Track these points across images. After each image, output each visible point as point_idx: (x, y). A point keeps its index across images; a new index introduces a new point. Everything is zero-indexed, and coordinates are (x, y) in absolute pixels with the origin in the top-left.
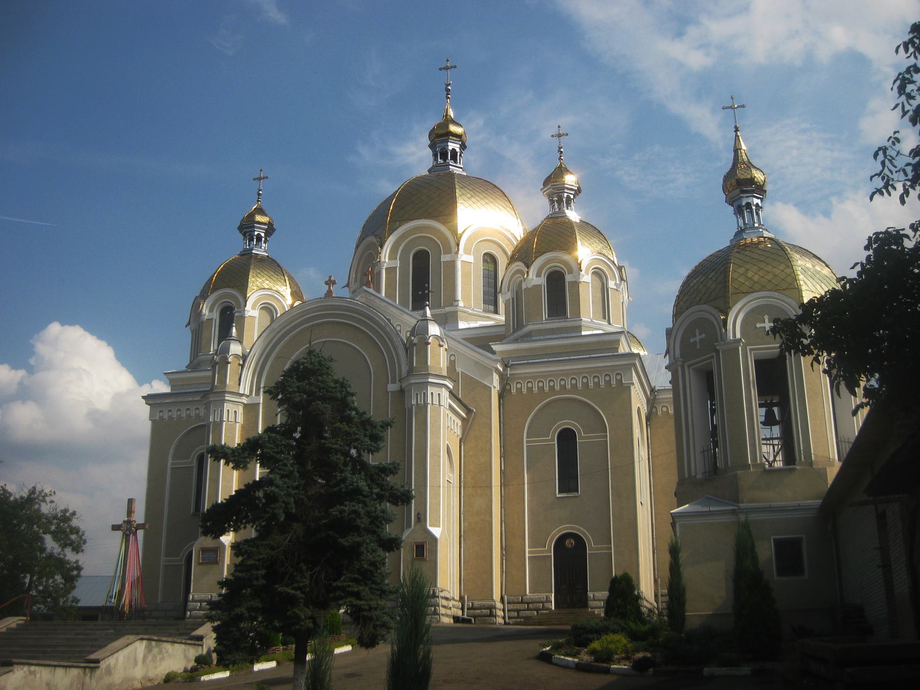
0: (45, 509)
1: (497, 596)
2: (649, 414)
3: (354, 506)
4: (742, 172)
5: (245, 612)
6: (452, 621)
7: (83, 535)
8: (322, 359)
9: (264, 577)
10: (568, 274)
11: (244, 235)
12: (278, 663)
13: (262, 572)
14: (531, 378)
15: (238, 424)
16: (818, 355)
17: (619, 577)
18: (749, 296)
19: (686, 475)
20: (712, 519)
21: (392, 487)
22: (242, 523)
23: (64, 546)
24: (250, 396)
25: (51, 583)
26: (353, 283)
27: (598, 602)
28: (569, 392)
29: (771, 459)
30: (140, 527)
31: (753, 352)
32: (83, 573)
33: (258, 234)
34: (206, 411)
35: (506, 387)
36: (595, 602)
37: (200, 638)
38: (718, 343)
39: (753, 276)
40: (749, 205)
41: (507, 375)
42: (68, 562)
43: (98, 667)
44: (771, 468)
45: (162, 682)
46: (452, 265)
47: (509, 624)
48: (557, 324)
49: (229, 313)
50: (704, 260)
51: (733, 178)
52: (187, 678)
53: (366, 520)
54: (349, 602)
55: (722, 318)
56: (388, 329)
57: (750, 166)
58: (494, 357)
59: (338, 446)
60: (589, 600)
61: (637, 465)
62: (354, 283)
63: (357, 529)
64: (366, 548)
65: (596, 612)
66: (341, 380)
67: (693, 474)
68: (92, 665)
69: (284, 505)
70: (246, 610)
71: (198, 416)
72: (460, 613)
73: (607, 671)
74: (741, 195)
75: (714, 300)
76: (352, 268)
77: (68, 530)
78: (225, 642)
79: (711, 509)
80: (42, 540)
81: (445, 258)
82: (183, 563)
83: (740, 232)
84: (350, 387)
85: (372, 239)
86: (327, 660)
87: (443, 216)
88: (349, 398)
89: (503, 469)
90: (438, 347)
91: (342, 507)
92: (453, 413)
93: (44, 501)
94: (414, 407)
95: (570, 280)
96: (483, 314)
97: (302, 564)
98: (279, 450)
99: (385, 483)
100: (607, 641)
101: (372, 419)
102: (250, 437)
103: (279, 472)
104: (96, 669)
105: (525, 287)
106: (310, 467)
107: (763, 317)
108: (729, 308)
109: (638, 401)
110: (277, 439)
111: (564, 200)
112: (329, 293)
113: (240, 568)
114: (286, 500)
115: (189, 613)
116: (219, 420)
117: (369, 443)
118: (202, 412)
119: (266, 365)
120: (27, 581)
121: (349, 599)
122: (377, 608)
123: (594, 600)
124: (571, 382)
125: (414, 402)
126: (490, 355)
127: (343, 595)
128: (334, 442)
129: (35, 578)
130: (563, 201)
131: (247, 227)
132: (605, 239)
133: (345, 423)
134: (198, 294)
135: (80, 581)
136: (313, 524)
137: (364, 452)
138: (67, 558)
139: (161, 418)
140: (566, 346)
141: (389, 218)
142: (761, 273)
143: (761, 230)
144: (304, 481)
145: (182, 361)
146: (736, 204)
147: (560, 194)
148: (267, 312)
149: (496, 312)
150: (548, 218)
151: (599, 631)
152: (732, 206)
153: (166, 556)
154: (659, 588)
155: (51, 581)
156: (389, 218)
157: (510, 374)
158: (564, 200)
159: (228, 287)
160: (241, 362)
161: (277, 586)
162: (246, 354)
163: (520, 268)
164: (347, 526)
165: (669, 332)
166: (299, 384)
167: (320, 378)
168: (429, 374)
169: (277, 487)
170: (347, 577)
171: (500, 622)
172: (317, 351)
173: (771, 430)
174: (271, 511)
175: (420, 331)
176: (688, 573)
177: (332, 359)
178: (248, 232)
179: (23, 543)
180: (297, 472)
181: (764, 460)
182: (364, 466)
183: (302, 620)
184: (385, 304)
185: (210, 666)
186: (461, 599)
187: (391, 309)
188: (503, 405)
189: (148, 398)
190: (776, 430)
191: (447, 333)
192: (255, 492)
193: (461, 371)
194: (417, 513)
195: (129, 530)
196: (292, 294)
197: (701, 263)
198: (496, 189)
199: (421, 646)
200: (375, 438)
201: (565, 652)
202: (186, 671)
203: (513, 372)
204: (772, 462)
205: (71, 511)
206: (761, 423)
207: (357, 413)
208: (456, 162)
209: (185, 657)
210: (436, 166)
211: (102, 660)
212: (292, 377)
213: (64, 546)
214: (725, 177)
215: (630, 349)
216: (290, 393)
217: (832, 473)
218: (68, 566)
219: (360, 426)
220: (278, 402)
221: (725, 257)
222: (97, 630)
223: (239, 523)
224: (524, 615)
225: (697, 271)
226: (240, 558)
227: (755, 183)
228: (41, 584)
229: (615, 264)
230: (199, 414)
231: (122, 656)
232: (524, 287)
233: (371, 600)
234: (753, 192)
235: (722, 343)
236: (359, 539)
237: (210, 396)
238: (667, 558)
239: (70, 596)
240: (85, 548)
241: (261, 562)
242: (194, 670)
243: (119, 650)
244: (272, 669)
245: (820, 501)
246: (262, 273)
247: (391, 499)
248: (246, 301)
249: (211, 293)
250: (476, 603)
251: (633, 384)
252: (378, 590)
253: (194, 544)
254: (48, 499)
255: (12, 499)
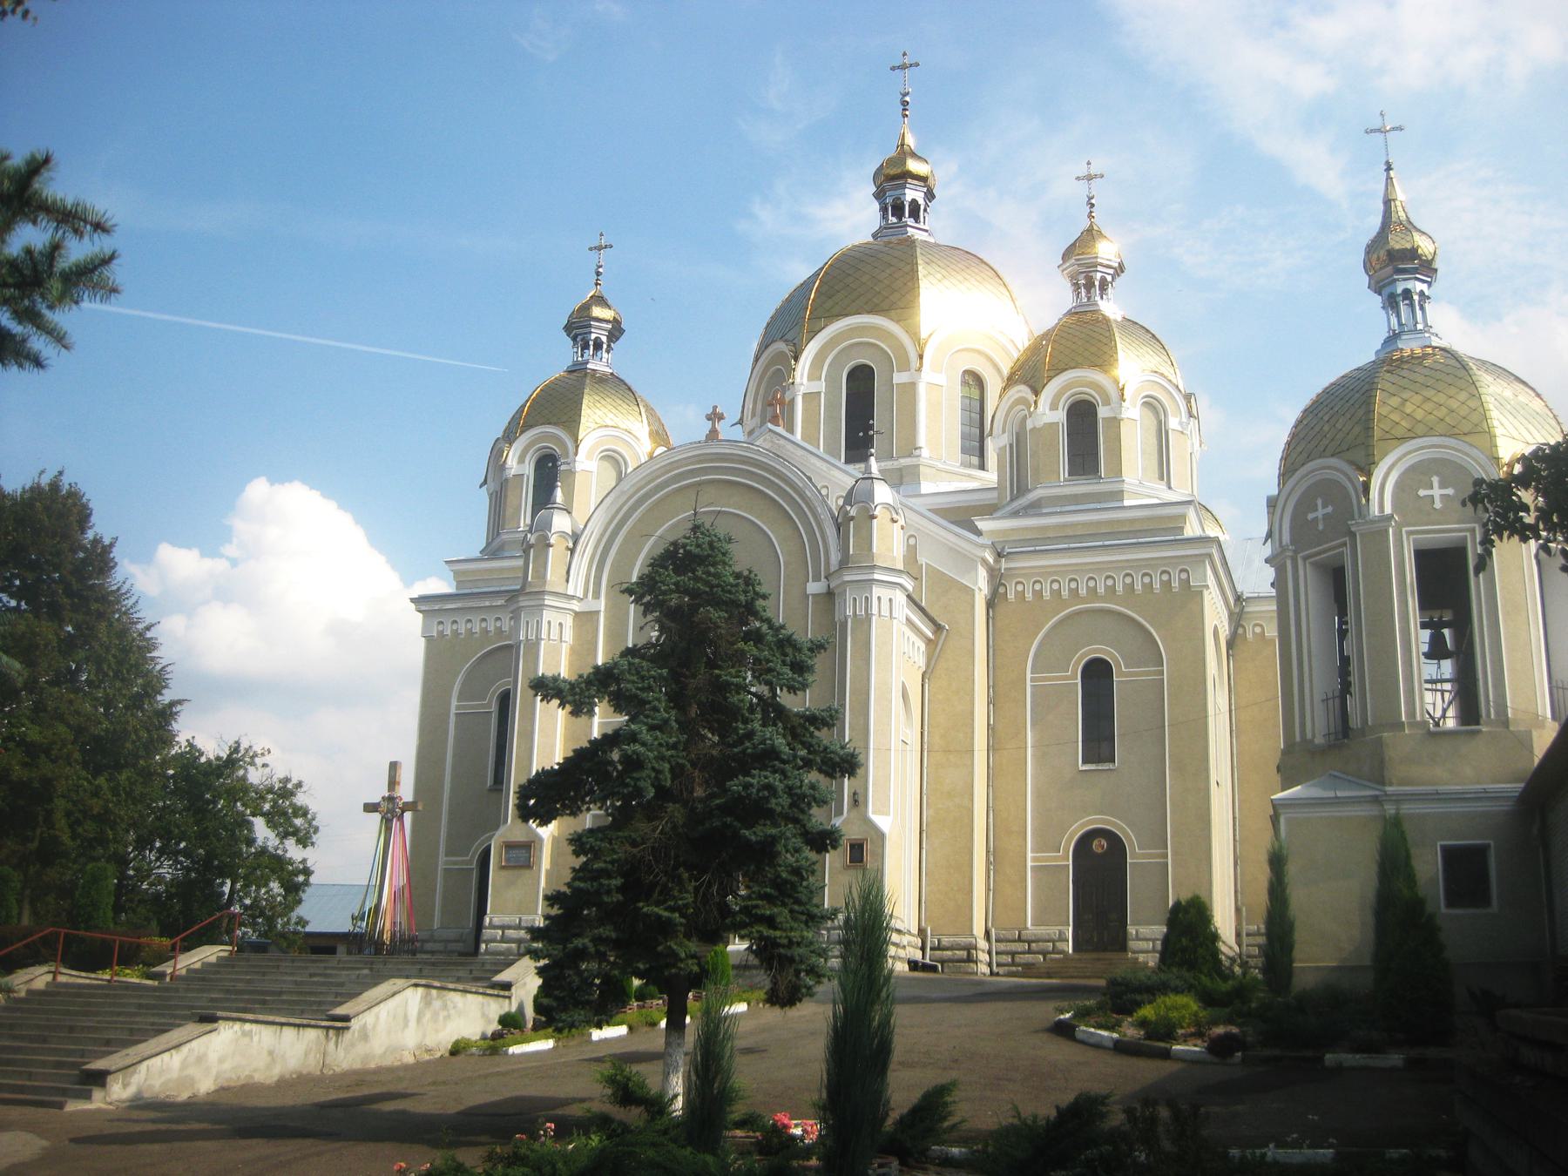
0: (255, 776)
1: (979, 929)
2: (1231, 636)
3: (766, 777)
4: (1398, 239)
5: (590, 945)
6: (906, 967)
7: (314, 819)
8: (714, 538)
9: (620, 889)
10: (1103, 405)
11: (574, 339)
12: (631, 1028)
13: (618, 882)
14: (1039, 574)
15: (564, 645)
16: (1548, 540)
17: (1183, 903)
18: (1407, 444)
19: (1298, 739)
20: (1339, 811)
21: (826, 748)
22: (584, 802)
23: (284, 836)
24: (585, 600)
25: (264, 894)
26: (750, 418)
27: (1145, 943)
28: (1084, 600)
29: (1438, 714)
30: (407, 807)
31: (1411, 537)
32: (312, 879)
33: (596, 338)
34: (512, 623)
35: (997, 590)
36: (1140, 943)
37: (507, 986)
38: (1353, 522)
39: (1414, 410)
40: (1407, 294)
41: (1000, 569)
42: (291, 862)
43: (348, 1028)
44: (1438, 729)
45: (447, 1054)
46: (911, 387)
47: (998, 974)
48: (1083, 487)
49: (550, 465)
50: (1332, 384)
51: (1382, 248)
52: (487, 1049)
53: (785, 801)
54: (758, 932)
55: (1361, 479)
56: (807, 492)
57: (1409, 227)
58: (980, 540)
59: (741, 679)
60: (1130, 940)
61: (1211, 720)
62: (752, 418)
63: (769, 815)
64: (785, 846)
65: (1141, 959)
66: (746, 573)
67: (1309, 736)
68: (339, 1024)
69: (653, 775)
70: (590, 941)
71: (499, 631)
72: (918, 955)
73: (1166, 1055)
74: (1396, 277)
75: (1348, 450)
76: (748, 394)
77: (290, 811)
78: (556, 992)
79: (1339, 794)
80: (249, 825)
81: (899, 378)
82: (474, 866)
83: (1393, 337)
84: (759, 584)
85: (781, 346)
86: (727, 1024)
87: (896, 309)
88: (760, 603)
89: (992, 722)
90: (890, 523)
91: (748, 779)
92: (917, 635)
93: (252, 764)
94: (849, 621)
95: (1106, 415)
96: (961, 470)
97: (682, 869)
98: (646, 685)
99: (814, 741)
100: (1165, 1006)
101: (794, 637)
102: (546, 674)
103: (645, 720)
104: (346, 1031)
105: (1032, 427)
106: (694, 711)
107: (1430, 478)
108: (1374, 463)
109: (1215, 615)
110: (642, 667)
111: (1097, 283)
112: (713, 434)
113: (581, 874)
114: (656, 765)
115: (483, 946)
116: (534, 638)
117: (790, 675)
118: (506, 625)
119: (611, 548)
120: (227, 889)
121: (757, 928)
122: (801, 942)
123: (1138, 938)
124: (1179, 576)
125: (849, 612)
126: (973, 537)
127: (747, 921)
128: (734, 673)
129: (238, 886)
130: (1094, 286)
131: (577, 327)
132: (1164, 348)
133: (752, 642)
134: (500, 435)
135: (309, 890)
136: (699, 806)
137: (781, 690)
138: (288, 855)
139: (441, 633)
140: (1099, 523)
141: (808, 313)
142: (1428, 406)
143: (1427, 335)
144: (685, 736)
145: (473, 540)
146: (1386, 291)
147: (1091, 274)
148: (609, 462)
149: (982, 467)
150: (1070, 313)
151: (1151, 990)
152: (1380, 294)
153: (446, 855)
154: (1244, 923)
155: (263, 891)
156: (808, 313)
157: (1005, 569)
158: (1097, 283)
159: (549, 424)
160: (571, 545)
161: (641, 904)
162: (579, 532)
163: (1024, 395)
164: (755, 810)
165: (1272, 503)
166: (678, 579)
167: (712, 570)
168: (874, 567)
169: (644, 744)
170: (754, 892)
171: (983, 971)
172: (707, 526)
173: (1439, 668)
174: (632, 783)
175: (860, 498)
176: (1299, 898)
177: (730, 539)
178: (580, 334)
179: (221, 831)
180: (676, 721)
181: (1427, 716)
182: (781, 712)
183: (681, 960)
184: (803, 452)
185: (523, 1031)
186: (922, 932)
187: (814, 460)
188: (993, 618)
189: (419, 601)
190: (1447, 667)
191: (904, 500)
192: (605, 752)
193: (926, 564)
194: (853, 791)
195: (392, 811)
196: (651, 434)
197: (1327, 388)
198: (983, 265)
199: (877, 1007)
200: (800, 668)
201: (1096, 1022)
202: (484, 1037)
203: (1012, 565)
204: (1439, 719)
205: (294, 781)
206: (1424, 654)
207: (771, 627)
208: (917, 220)
209: (484, 1015)
210: (885, 228)
211: (354, 1017)
212: (667, 569)
213: (284, 836)
214: (1368, 246)
215: (1203, 530)
216: (664, 593)
217: (1544, 739)
218: (291, 868)
219: (775, 648)
220: (643, 607)
221: (1367, 380)
222: (343, 969)
223: (579, 803)
224: (1022, 961)
225: (1321, 401)
226: (583, 859)
227: (1419, 257)
228: (247, 895)
229: (1180, 391)
230: (501, 627)
231: (384, 1010)
232: (1029, 425)
233: (792, 929)
234: (1415, 271)
235: (1360, 521)
236: (774, 831)
237: (521, 599)
238: (1263, 875)
239: (294, 916)
240: (317, 840)
241: (616, 865)
242: (496, 1036)
243: (380, 1002)
244: (619, 1039)
245: (1522, 785)
246: (602, 401)
247: (824, 768)
248: (577, 447)
249: (522, 432)
250: (946, 941)
251: (1207, 587)
252: (802, 913)
253: (494, 835)
254: (259, 761)
255: (203, 760)
